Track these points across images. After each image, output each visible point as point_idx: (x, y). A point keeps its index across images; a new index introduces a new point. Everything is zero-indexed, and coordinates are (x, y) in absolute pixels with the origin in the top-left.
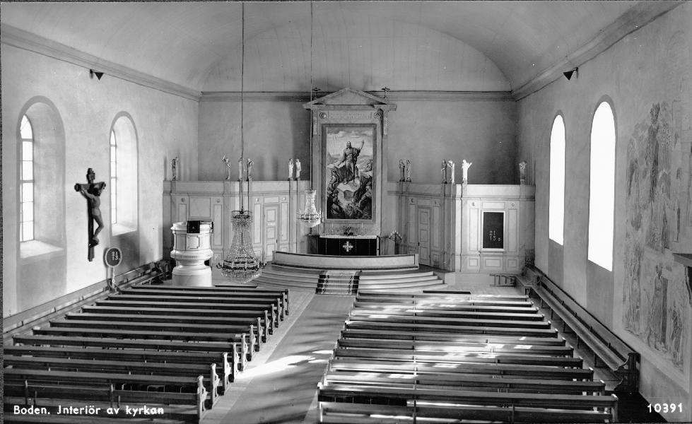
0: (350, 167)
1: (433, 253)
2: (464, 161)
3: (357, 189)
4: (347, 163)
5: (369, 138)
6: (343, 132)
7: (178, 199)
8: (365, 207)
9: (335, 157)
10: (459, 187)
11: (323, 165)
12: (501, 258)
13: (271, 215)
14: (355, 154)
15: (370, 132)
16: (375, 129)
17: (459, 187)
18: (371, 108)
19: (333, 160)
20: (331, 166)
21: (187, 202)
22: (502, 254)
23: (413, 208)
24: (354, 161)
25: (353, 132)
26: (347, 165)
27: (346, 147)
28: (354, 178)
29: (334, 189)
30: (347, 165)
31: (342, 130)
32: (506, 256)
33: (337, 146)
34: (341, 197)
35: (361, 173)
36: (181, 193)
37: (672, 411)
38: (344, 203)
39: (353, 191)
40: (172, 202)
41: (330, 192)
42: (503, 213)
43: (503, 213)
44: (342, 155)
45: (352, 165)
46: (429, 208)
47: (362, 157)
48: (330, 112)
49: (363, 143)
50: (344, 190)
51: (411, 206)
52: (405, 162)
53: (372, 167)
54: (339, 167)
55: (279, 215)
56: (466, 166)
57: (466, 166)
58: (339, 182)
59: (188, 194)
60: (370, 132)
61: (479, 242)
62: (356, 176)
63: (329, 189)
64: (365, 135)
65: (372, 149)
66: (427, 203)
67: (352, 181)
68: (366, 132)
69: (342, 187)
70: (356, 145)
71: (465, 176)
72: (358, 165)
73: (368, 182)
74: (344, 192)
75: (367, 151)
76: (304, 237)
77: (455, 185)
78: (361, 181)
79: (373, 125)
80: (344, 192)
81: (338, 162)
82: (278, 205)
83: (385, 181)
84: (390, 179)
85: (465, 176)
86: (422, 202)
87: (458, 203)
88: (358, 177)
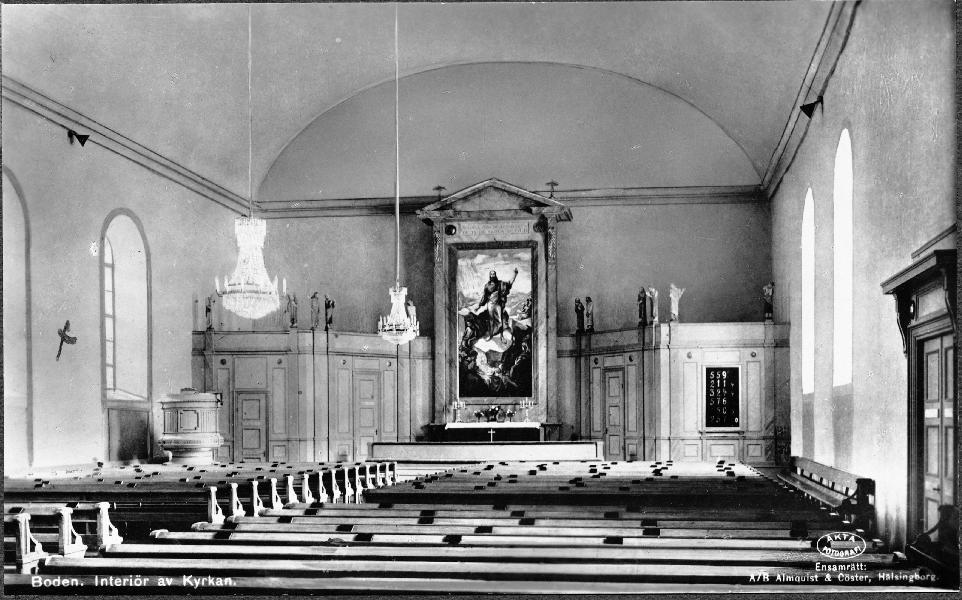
0: (495, 312)
1: (627, 442)
2: (673, 286)
3: (506, 347)
4: (489, 306)
5: (526, 265)
6: (484, 256)
7: (216, 360)
8: (519, 382)
9: (471, 296)
10: (664, 328)
11: (451, 309)
12: (736, 442)
13: (366, 387)
14: (498, 289)
15: (526, 255)
16: (534, 249)
17: (664, 328)
18: (525, 214)
19: (468, 301)
20: (465, 312)
21: (229, 364)
22: (737, 435)
23: (596, 374)
24: (501, 302)
25: (500, 255)
26: (490, 309)
27: (488, 280)
28: (501, 331)
29: (469, 351)
30: (490, 309)
31: (482, 254)
32: (744, 438)
33: (472, 284)
34: (481, 361)
35: (514, 322)
36: (219, 352)
37: (891, 503)
38: (487, 372)
39: (501, 351)
40: (206, 365)
41: (464, 354)
42: (737, 369)
43: (737, 369)
44: (481, 294)
45: (498, 309)
46: (621, 369)
47: (512, 297)
48: (462, 224)
49: (516, 272)
50: (486, 350)
51: (595, 370)
52: (583, 301)
53: (531, 312)
54: (477, 313)
55: (379, 395)
56: (675, 295)
57: (675, 295)
58: (478, 337)
59: (232, 353)
60: (526, 255)
61: (700, 416)
62: (505, 326)
63: (462, 349)
64: (519, 259)
65: (529, 282)
66: (619, 361)
67: (499, 335)
68: (519, 255)
69: (483, 345)
70: (504, 276)
71: (675, 310)
72: (508, 309)
73: (525, 338)
74: (487, 354)
75: (522, 286)
76: (422, 428)
77: (658, 326)
78: (513, 334)
79: (530, 245)
80: (487, 354)
81: (477, 306)
82: (378, 373)
83: (553, 336)
84: (561, 331)
85: (675, 310)
86: (609, 362)
87: (664, 354)
88: (508, 328)
